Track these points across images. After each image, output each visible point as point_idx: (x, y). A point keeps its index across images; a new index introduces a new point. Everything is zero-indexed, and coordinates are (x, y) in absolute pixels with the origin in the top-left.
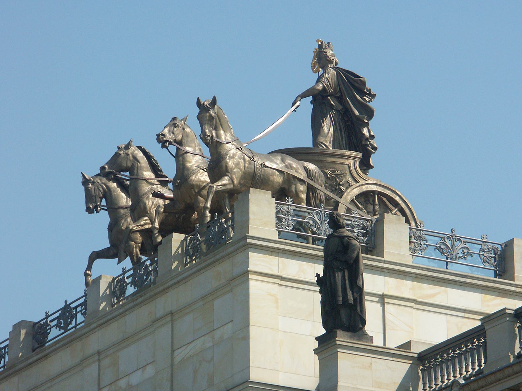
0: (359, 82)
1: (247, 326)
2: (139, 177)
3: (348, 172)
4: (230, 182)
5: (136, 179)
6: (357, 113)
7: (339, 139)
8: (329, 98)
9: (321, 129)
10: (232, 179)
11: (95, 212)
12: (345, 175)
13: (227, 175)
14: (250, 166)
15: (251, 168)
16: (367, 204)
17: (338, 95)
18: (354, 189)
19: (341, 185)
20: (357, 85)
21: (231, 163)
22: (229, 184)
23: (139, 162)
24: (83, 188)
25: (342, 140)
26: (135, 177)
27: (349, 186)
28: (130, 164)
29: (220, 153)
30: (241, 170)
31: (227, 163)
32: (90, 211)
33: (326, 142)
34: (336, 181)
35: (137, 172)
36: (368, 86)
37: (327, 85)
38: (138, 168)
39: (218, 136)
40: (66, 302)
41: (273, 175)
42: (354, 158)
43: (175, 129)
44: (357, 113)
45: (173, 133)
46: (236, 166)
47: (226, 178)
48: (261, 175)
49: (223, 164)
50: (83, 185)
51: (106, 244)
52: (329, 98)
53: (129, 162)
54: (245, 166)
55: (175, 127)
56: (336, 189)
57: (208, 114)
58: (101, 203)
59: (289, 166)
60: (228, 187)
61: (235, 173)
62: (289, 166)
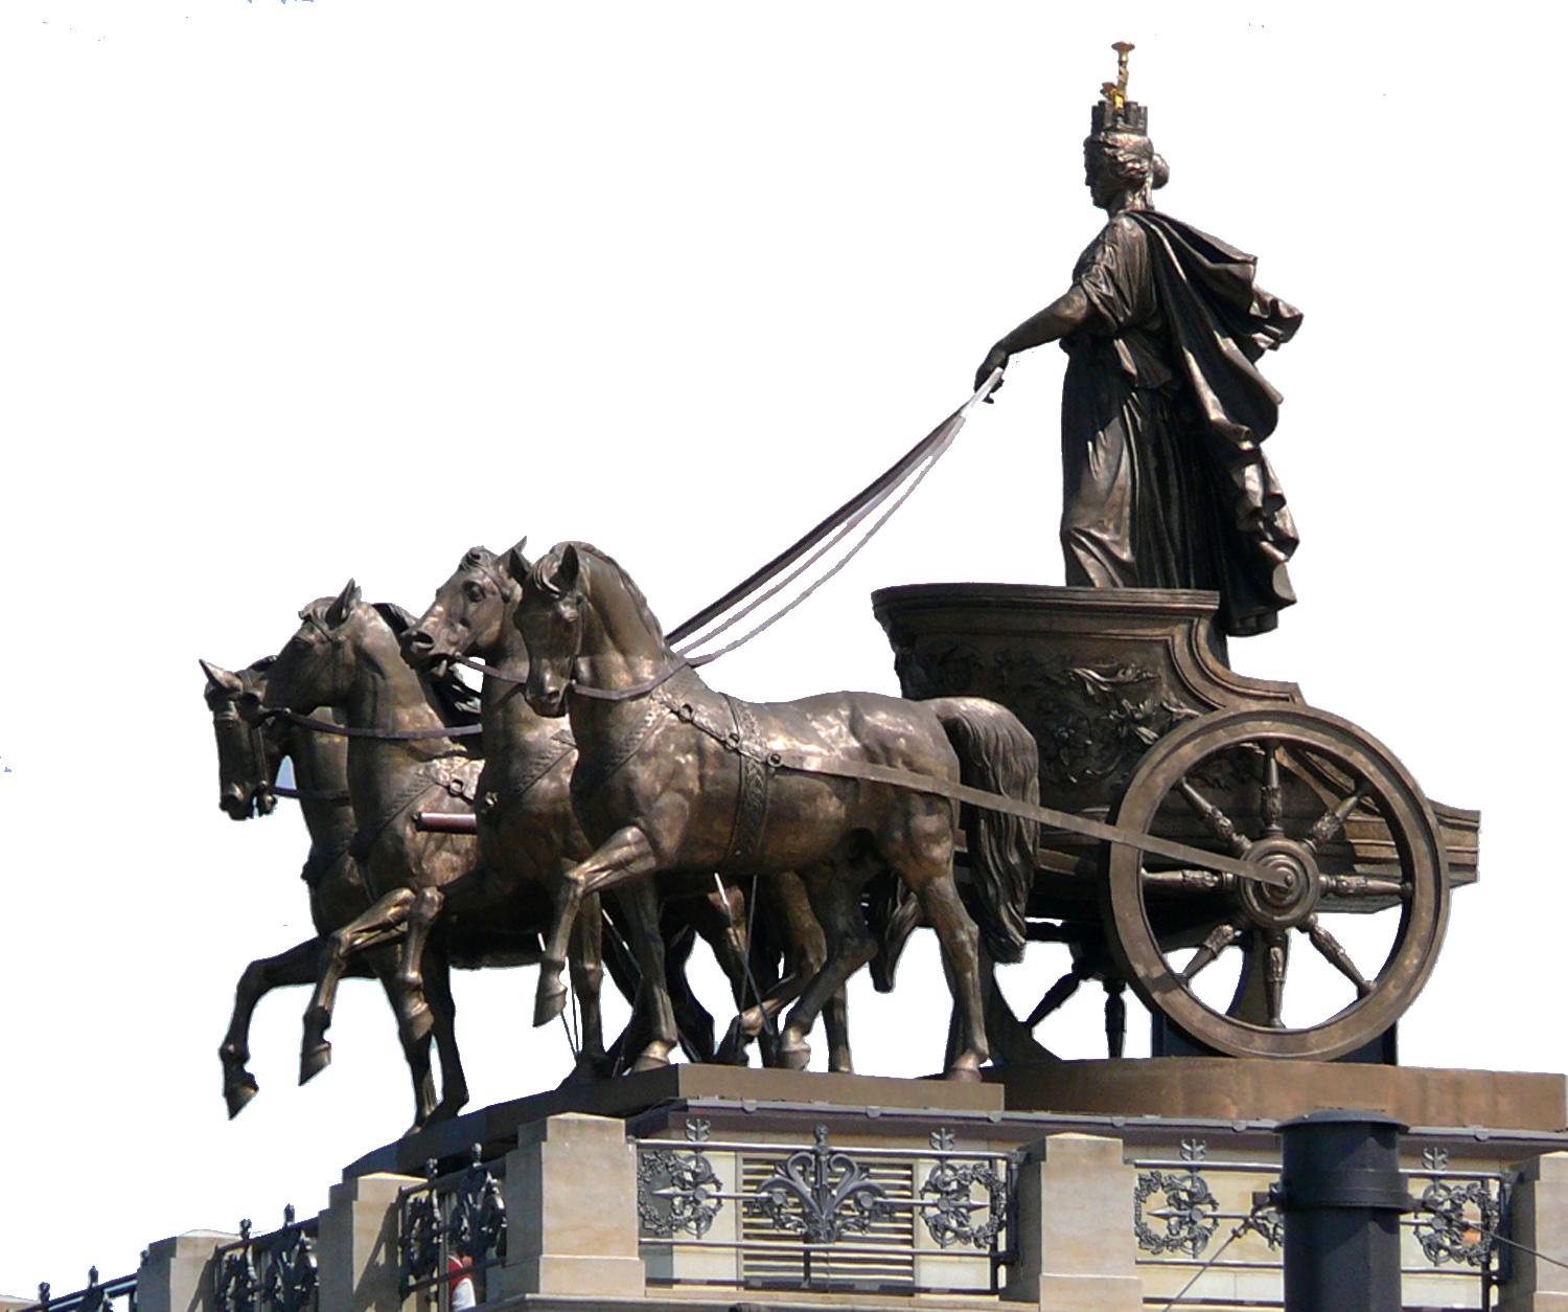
0: (1225, 277)
1: (1034, 1013)
2: (380, 733)
3: (1163, 672)
4: (646, 846)
5: (366, 738)
6: (1216, 414)
7: (1154, 511)
8: (1120, 344)
9: (1085, 474)
10: (650, 836)
11: (256, 811)
12: (1153, 683)
13: (635, 824)
14: (721, 773)
15: (725, 782)
16: (1243, 782)
17: (1156, 325)
18: (1179, 745)
19: (1140, 723)
20: (1217, 288)
21: (644, 776)
22: (640, 856)
23: (377, 668)
24: (210, 716)
25: (1166, 507)
26: (369, 732)
27: (1167, 724)
28: (344, 683)
29: (608, 737)
30: (686, 793)
31: (630, 779)
32: (237, 809)
33: (1104, 530)
34: (1121, 709)
35: (374, 710)
36: (1265, 281)
37: (1105, 299)
38: (375, 694)
39: (597, 679)
40: (94, 1275)
41: (811, 797)
42: (1188, 616)
43: (472, 607)
44: (1216, 414)
45: (464, 622)
46: (665, 787)
47: (631, 834)
48: (763, 802)
49: (617, 781)
50: (212, 706)
51: (305, 930)
52: (1120, 344)
53: (342, 672)
54: (701, 778)
55: (473, 598)
56: (1119, 740)
57: (550, 614)
58: (273, 778)
59: (878, 750)
60: (639, 867)
61: (661, 812)
62: (878, 750)
